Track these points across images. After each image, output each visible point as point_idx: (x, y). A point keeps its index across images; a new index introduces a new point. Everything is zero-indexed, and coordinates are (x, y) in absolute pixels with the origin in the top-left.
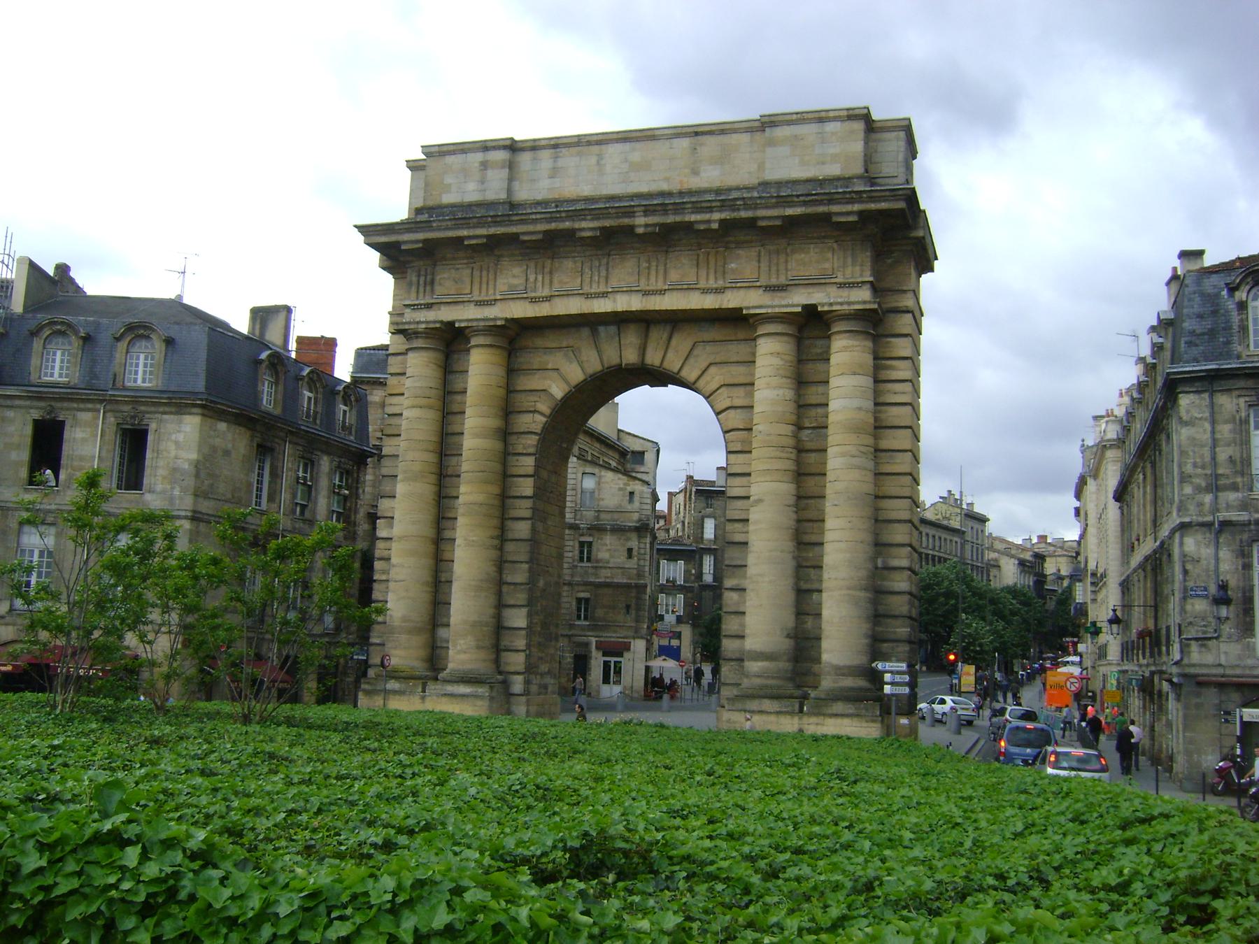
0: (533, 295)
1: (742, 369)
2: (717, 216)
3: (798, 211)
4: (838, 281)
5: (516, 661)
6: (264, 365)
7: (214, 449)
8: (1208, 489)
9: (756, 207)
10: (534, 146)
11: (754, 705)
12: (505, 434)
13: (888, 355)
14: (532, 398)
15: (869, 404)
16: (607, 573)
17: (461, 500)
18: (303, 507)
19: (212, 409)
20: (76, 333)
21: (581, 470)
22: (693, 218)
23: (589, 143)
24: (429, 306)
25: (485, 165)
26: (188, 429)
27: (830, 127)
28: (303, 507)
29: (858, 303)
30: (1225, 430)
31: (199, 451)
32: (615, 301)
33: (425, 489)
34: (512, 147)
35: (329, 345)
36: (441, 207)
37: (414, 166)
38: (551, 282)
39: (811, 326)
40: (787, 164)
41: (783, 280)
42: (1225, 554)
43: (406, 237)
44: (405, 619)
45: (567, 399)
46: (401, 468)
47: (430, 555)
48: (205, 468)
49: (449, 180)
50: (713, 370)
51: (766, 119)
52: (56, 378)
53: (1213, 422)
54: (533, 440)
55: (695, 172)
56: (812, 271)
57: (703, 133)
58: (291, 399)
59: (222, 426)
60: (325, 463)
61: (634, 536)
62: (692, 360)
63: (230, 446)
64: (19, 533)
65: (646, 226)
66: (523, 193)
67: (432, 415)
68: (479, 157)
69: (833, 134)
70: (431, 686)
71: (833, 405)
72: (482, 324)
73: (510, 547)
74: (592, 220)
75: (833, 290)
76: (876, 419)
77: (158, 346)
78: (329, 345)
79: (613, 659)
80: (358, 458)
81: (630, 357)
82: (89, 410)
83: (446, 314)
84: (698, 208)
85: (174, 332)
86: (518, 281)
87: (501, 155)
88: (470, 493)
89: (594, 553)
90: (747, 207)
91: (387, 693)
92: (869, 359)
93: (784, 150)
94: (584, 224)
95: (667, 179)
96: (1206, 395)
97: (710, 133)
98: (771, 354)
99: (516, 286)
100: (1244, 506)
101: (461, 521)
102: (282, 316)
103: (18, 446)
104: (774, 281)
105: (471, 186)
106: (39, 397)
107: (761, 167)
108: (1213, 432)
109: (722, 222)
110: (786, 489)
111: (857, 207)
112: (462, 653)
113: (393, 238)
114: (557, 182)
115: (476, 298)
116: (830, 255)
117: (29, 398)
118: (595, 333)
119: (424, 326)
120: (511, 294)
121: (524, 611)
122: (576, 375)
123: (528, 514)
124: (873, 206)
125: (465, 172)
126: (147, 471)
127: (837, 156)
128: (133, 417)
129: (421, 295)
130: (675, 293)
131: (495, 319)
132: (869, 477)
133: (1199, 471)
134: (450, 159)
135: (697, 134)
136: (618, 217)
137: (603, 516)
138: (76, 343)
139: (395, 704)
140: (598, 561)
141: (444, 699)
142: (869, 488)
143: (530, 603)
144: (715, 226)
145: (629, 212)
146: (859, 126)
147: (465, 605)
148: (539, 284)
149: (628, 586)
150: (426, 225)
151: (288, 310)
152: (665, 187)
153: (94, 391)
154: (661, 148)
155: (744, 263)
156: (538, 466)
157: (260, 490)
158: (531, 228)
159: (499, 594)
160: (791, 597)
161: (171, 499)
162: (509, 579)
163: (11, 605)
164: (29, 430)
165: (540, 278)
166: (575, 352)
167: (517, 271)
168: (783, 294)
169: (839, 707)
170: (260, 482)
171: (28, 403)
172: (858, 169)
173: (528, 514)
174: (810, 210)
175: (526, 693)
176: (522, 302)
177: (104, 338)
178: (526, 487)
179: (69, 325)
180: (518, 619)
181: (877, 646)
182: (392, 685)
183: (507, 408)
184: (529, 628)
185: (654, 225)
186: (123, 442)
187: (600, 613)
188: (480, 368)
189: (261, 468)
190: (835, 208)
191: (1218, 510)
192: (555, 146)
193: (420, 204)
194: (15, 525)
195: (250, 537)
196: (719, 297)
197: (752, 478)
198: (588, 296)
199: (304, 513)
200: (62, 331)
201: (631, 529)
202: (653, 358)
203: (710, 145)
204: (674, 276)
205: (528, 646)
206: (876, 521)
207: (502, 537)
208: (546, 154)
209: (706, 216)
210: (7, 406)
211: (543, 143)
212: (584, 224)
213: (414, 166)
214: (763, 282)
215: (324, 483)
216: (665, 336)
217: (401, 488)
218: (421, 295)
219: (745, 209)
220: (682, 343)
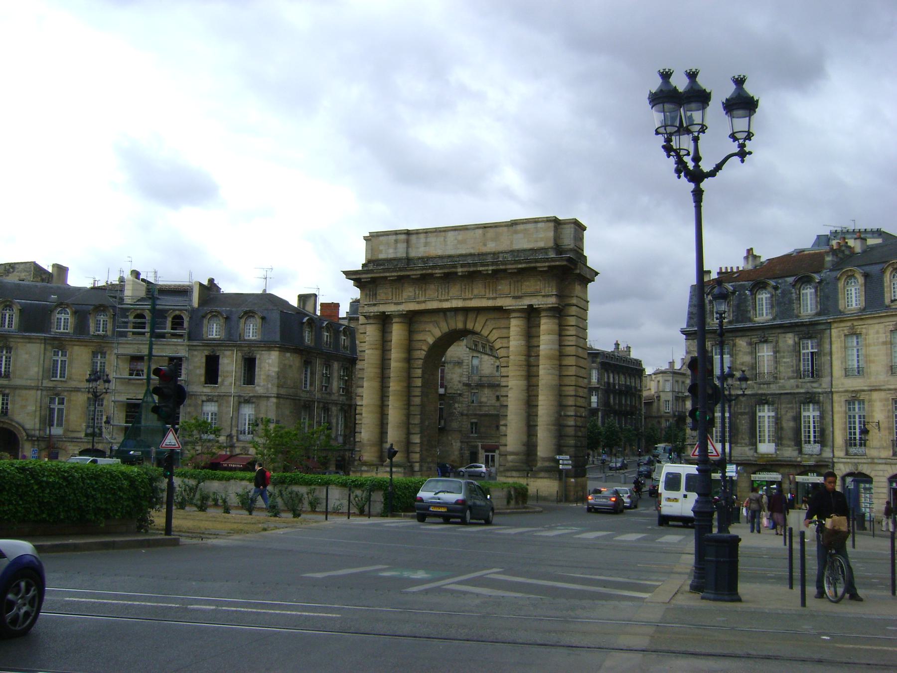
1: (505, 331)
2: (491, 268)
3: (523, 266)
4: (543, 296)
5: (416, 457)
7: (285, 365)
10: (417, 232)
11: (509, 474)
12: (409, 360)
15: (557, 347)
16: (486, 409)
17: (391, 389)
18: (326, 387)
19: (283, 349)
20: (222, 315)
21: (471, 355)
22: (481, 269)
24: (375, 305)
25: (396, 241)
26: (273, 357)
27: (540, 225)
28: (326, 387)
31: (279, 367)
33: (376, 384)
34: (408, 233)
35: (337, 306)
37: (366, 238)
39: (531, 314)
41: (520, 294)
43: (364, 276)
44: (368, 440)
46: (366, 375)
47: (379, 412)
48: (281, 374)
49: (381, 248)
50: (494, 331)
52: (214, 336)
54: (420, 362)
55: (485, 245)
56: (531, 290)
58: (318, 337)
59: (288, 355)
60: (336, 366)
64: (202, 405)
66: (413, 254)
67: (378, 352)
68: (394, 237)
70: (380, 469)
71: (542, 347)
73: (412, 408)
75: (540, 298)
76: (560, 352)
77: (259, 321)
78: (337, 306)
79: (490, 454)
80: (350, 361)
81: (460, 326)
83: (382, 308)
85: (265, 314)
86: (412, 294)
87: (403, 237)
88: (394, 386)
90: (503, 265)
91: (362, 471)
92: (556, 328)
93: (521, 236)
94: (437, 271)
95: (473, 248)
97: (491, 227)
98: (516, 325)
101: (391, 398)
102: (313, 299)
103: (200, 368)
104: (516, 294)
105: (391, 251)
106: (208, 345)
107: (512, 243)
110: (522, 383)
111: (547, 264)
113: (358, 276)
114: (427, 249)
118: (445, 315)
120: (409, 300)
121: (419, 436)
122: (438, 333)
123: (419, 394)
124: (553, 264)
125: (388, 244)
126: (257, 377)
127: (544, 238)
132: (557, 378)
134: (381, 238)
137: (483, 379)
138: (222, 321)
139: (365, 475)
142: (556, 382)
143: (421, 432)
146: (552, 225)
150: (371, 271)
151: (315, 296)
152: (472, 251)
153: (233, 340)
154: (470, 234)
155: (504, 286)
156: (423, 373)
157: (306, 381)
158: (415, 273)
159: (408, 429)
160: (525, 429)
161: (267, 389)
162: (412, 422)
164: (204, 360)
166: (437, 324)
167: (411, 289)
169: (542, 474)
170: (306, 377)
172: (551, 244)
173: (419, 394)
174: (528, 265)
175: (421, 470)
177: (235, 317)
178: (419, 382)
179: (219, 312)
180: (416, 439)
181: (560, 450)
182: (364, 468)
183: (409, 348)
184: (421, 443)
186: (245, 363)
187: (483, 429)
188: (397, 332)
189: (306, 371)
190: (538, 265)
192: (426, 233)
193: (369, 257)
194: (200, 402)
195: (302, 403)
197: (509, 379)
198: (441, 301)
199: (327, 388)
200: (216, 315)
202: (470, 326)
203: (491, 233)
204: (476, 292)
205: (421, 451)
206: (560, 396)
207: (408, 404)
208: (422, 236)
212: (437, 271)
213: (366, 238)
214: (512, 294)
215: (335, 375)
217: (365, 384)
220: (481, 319)
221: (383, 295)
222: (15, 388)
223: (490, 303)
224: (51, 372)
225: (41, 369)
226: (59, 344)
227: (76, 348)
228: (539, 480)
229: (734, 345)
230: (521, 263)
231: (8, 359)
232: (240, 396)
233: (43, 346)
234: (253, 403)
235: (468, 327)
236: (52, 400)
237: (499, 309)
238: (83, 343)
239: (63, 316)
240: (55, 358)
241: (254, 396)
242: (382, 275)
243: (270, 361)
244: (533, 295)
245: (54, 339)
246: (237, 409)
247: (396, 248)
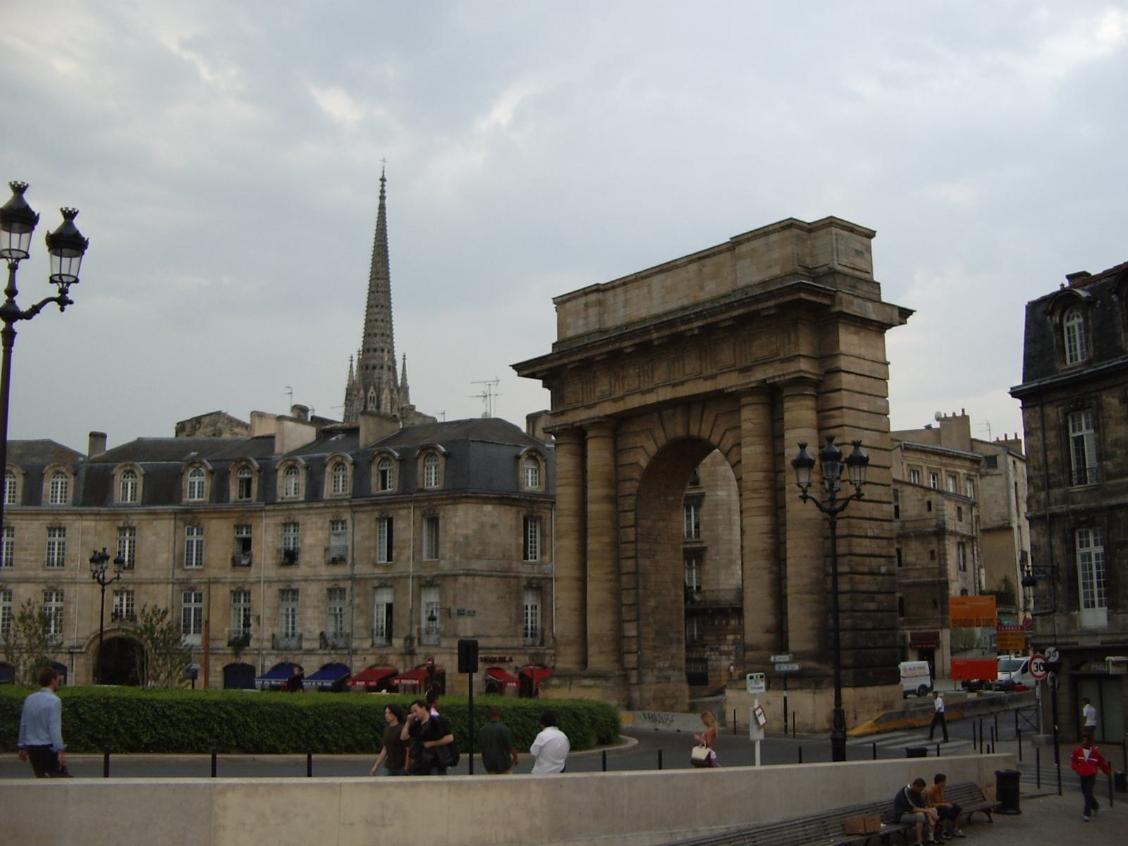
3: (741, 311)
6: (523, 459)
8: (1042, 489)
13: (828, 407)
22: (683, 328)
25: (586, 306)
27: (773, 237)
29: (794, 373)
30: (1051, 435)
34: (598, 289)
38: (623, 385)
40: (750, 274)
42: (1056, 542)
45: (650, 465)
50: (728, 434)
51: (734, 240)
53: (1044, 431)
54: (631, 501)
55: (702, 288)
59: (488, 508)
61: (934, 540)
63: (497, 521)
65: (659, 338)
75: (778, 365)
82: (405, 508)
89: (903, 558)
95: (686, 296)
96: (1038, 409)
97: (708, 256)
98: (751, 417)
100: (1067, 499)
103: (322, 528)
104: (744, 364)
108: (1044, 438)
111: (772, 303)
112: (599, 659)
115: (585, 403)
116: (774, 339)
117: (372, 504)
122: (652, 448)
124: (781, 300)
128: (430, 510)
133: (1036, 473)
135: (700, 259)
137: (907, 525)
140: (907, 564)
144: (696, 332)
145: (646, 331)
147: (599, 624)
149: (933, 584)
152: (685, 302)
158: (599, 351)
163: (373, 642)
168: (749, 374)
171: (372, 508)
185: (663, 337)
188: (598, 453)
190: (761, 306)
191: (1050, 505)
194: (370, 589)
195: (524, 583)
198: (674, 385)
201: (930, 534)
202: (694, 431)
204: (688, 369)
208: (620, 290)
210: (361, 512)
211: (617, 283)
222: (140, 583)
224: (183, 559)
225: (172, 556)
226: (191, 518)
227: (214, 522)
229: (1100, 407)
230: (734, 309)
231: (132, 543)
232: (420, 577)
233: (173, 522)
234: (438, 586)
235: (691, 433)
236: (187, 599)
237: (719, 396)
238: (220, 514)
239: (197, 479)
240: (190, 538)
241: (438, 576)
243: (457, 520)
244: (765, 362)
245: (186, 512)
246: (417, 598)
247: (586, 318)
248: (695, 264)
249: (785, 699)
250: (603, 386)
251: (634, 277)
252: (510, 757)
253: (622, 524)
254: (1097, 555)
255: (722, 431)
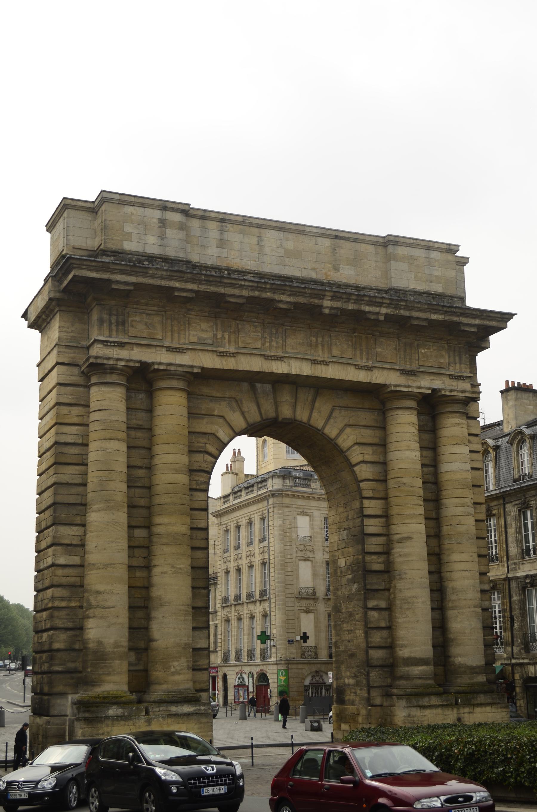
0: (221, 349)
2: (384, 310)
9: (412, 309)
10: (204, 216)
11: (425, 701)
14: (201, 440)
22: (367, 309)
23: (251, 225)
25: (163, 223)
27: (434, 255)
32: (289, 365)
34: (186, 211)
36: (124, 252)
41: (414, 367)
49: (128, 228)
57: (341, 238)
62: (332, 421)
65: (332, 308)
69: (436, 260)
72: (180, 369)
74: (290, 295)
84: (372, 302)
93: (403, 266)
94: (283, 298)
95: (315, 269)
97: (346, 239)
99: (205, 339)
104: (408, 367)
105: (152, 240)
109: (386, 315)
111: (477, 322)
114: (224, 253)
119: (123, 363)
129: (114, 333)
130: (336, 366)
131: (192, 367)
134: (129, 209)
135: (336, 237)
136: (311, 297)
141: (170, 720)
148: (226, 341)
154: (307, 243)
158: (236, 292)
165: (226, 336)
167: (204, 325)
168: (414, 378)
176: (210, 354)
188: (171, 408)
190: (464, 320)
196: (369, 373)
198: (268, 358)
203: (346, 248)
204: (336, 352)
209: (377, 310)
211: (213, 215)
212: (283, 298)
216: (310, 398)
218: (114, 333)
219: (405, 309)
221: (141, 327)
223: (362, 376)
228: (478, 710)
242: (163, 283)
248: (329, 240)
249: (24, 702)
250: (138, 324)
251: (241, 219)
252: (383, 805)
253: (383, 520)
254: (494, 600)
255: (341, 425)
